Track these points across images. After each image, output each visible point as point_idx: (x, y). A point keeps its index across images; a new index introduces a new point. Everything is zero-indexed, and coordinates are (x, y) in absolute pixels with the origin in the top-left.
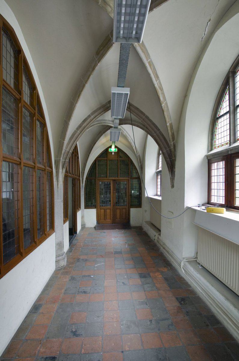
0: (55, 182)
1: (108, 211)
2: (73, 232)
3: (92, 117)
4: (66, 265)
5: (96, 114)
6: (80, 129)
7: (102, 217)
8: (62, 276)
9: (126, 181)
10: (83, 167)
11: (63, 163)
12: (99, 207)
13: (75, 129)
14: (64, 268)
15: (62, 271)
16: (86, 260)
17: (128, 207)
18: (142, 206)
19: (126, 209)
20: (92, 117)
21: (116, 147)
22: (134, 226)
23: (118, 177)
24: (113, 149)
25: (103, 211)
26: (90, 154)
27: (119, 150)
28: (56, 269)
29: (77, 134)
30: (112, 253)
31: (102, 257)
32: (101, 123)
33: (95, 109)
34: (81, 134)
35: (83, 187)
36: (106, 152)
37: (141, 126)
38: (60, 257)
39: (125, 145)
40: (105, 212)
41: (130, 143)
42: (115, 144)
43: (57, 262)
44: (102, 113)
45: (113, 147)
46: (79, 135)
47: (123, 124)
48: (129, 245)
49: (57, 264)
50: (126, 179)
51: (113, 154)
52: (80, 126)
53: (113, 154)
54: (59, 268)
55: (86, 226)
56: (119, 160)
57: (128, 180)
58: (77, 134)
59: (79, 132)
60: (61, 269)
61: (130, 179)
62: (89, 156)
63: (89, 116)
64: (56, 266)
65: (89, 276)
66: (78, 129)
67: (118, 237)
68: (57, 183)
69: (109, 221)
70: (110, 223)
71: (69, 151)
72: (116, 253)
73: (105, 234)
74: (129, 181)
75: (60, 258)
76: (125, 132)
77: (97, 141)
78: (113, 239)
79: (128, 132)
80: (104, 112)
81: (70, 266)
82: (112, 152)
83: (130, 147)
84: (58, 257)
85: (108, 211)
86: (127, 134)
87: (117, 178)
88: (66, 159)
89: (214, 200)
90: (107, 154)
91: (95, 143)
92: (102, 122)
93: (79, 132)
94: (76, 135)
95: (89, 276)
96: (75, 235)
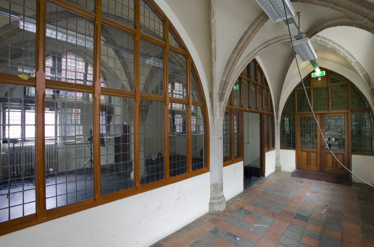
0: (210, 116)
1: (313, 155)
2: (260, 174)
3: (250, 32)
4: (223, 211)
5: (254, 26)
6: (237, 52)
7: (304, 162)
8: (208, 223)
9: (343, 114)
10: (277, 101)
11: (221, 94)
12: (299, 148)
13: (231, 54)
14: (218, 214)
15: (213, 216)
16: (250, 213)
17: (348, 153)
18: (281, 150)
19: (343, 155)
20: (250, 32)
21: (322, 69)
22: (358, 181)
23: (328, 110)
24: (318, 73)
25: (305, 154)
26: (283, 83)
27: (329, 72)
28: (209, 211)
29: (233, 59)
30: (292, 214)
31: (273, 215)
32: (282, 40)
33: (253, 20)
34: (238, 57)
35: (278, 123)
36: (308, 79)
37: (348, 21)
38: (215, 200)
39: (340, 64)
40: (308, 155)
41: (345, 58)
42: (318, 66)
43: (211, 204)
44: (262, 23)
45: (318, 70)
46: (236, 59)
47: (318, 32)
48: (330, 211)
49: (211, 207)
50: (343, 111)
51: (319, 79)
52: (236, 49)
53: (319, 79)
54: (213, 212)
55: (282, 169)
56: (329, 87)
57: (346, 114)
58: (233, 59)
59: (235, 55)
60: (215, 213)
61: (350, 112)
62: (282, 86)
63: (246, 32)
64: (210, 208)
65: (235, 236)
66: (233, 53)
67: (318, 192)
68: (212, 118)
69: (314, 167)
70: (316, 171)
71: (226, 81)
72: (299, 217)
73: (301, 184)
74: (349, 115)
75: (216, 201)
76: (331, 43)
77: (289, 67)
78: (308, 194)
79: (335, 41)
80: (265, 20)
81: (226, 213)
82: (317, 78)
83: (349, 66)
84: (213, 199)
85: (313, 155)
86: (335, 46)
87: (327, 111)
88: (223, 91)
89: (8, 112)
90: (310, 81)
91: (288, 69)
92: (283, 38)
93: (235, 55)
94: (232, 60)
95: (235, 236)
96: (262, 177)
